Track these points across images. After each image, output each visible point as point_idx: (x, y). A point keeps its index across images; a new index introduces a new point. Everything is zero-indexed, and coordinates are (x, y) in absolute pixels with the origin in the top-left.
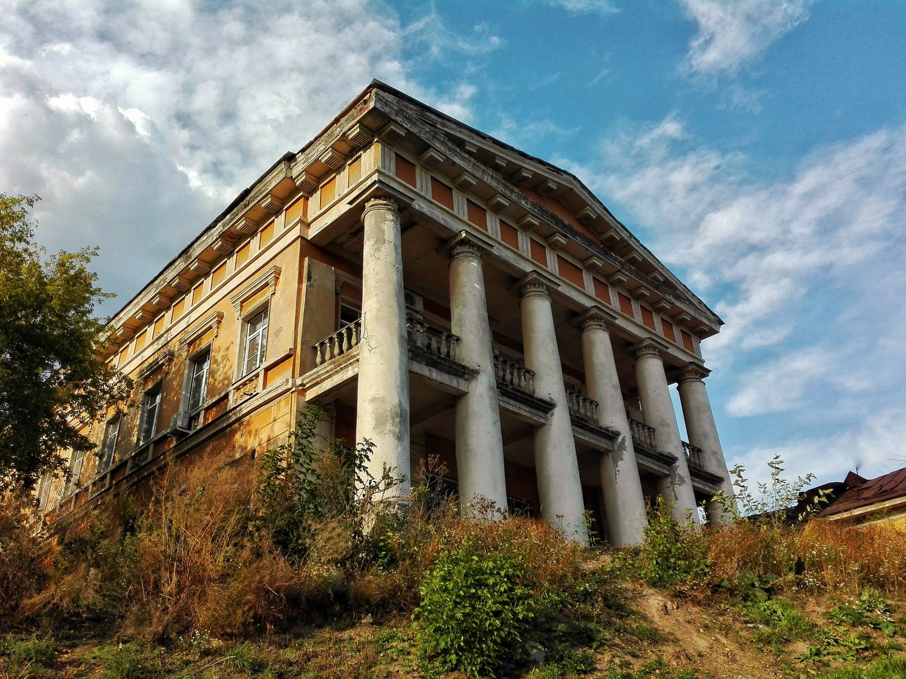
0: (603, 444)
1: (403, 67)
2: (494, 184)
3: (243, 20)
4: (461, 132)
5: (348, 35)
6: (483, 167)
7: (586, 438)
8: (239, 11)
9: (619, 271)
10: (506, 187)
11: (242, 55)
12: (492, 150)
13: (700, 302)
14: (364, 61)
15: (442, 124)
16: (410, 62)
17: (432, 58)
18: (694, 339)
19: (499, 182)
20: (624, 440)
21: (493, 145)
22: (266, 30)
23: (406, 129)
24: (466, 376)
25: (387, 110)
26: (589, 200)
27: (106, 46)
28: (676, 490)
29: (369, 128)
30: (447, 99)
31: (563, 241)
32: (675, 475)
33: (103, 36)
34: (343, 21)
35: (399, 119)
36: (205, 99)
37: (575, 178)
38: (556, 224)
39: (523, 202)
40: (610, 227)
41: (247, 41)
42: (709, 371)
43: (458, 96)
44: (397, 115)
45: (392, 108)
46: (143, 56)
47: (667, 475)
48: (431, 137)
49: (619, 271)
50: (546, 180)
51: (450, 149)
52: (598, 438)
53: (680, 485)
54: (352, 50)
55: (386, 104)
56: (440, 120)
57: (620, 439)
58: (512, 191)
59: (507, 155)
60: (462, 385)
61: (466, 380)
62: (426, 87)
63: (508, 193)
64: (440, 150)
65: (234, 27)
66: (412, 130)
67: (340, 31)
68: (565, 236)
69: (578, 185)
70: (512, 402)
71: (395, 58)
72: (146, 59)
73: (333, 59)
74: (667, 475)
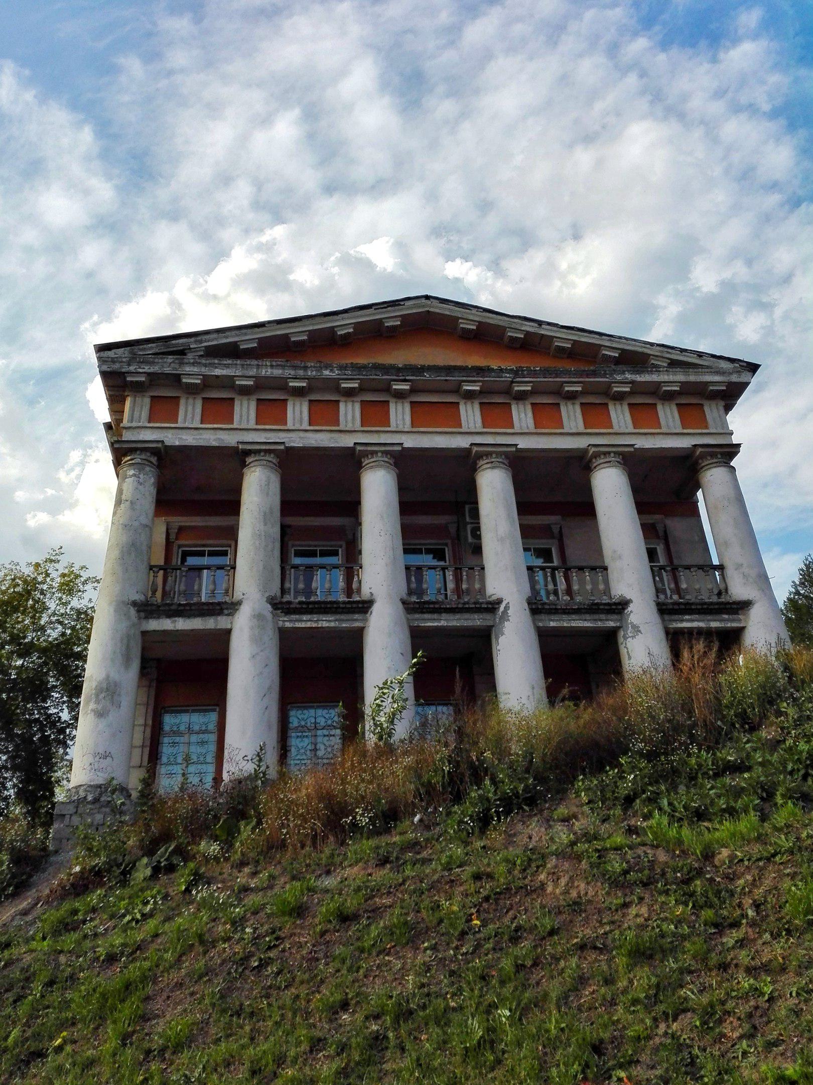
0: (476, 621)
1: (650, 38)
2: (277, 372)
3: (450, 94)
4: (227, 337)
5: (569, 43)
6: (254, 362)
7: (443, 623)
8: (441, 89)
9: (512, 382)
10: (295, 367)
11: (467, 130)
12: (279, 333)
13: (700, 355)
14: (600, 59)
15: (196, 342)
16: (657, 28)
17: (681, 8)
18: (711, 411)
19: (283, 367)
20: (507, 608)
21: (279, 326)
22: (477, 91)
23: (145, 373)
24: (226, 612)
25: (116, 366)
26: (458, 312)
27: (336, 197)
28: (629, 645)
29: (118, 387)
30: (728, 43)
31: (406, 387)
32: (627, 624)
33: (330, 189)
34: (554, 31)
35: (132, 368)
36: (454, 193)
37: (427, 297)
38: (387, 374)
39: (327, 372)
40: (504, 329)
41: (464, 115)
42: (739, 445)
43: (741, 31)
44: (129, 365)
45: (122, 362)
46: (373, 187)
47: (619, 628)
48: (177, 366)
49: (512, 382)
50: (380, 322)
51: (205, 365)
52: (467, 616)
53: (633, 637)
54: (581, 55)
55: (113, 361)
56: (193, 339)
57: (502, 608)
58: (305, 368)
59: (304, 326)
60: (222, 622)
61: (228, 615)
62: (694, 45)
63: (301, 373)
64: (192, 373)
65: (446, 108)
66: (152, 370)
67: (556, 43)
68: (405, 380)
69: (435, 302)
70: (305, 617)
71: (635, 34)
72: (379, 188)
73: (564, 80)
74: (619, 628)
